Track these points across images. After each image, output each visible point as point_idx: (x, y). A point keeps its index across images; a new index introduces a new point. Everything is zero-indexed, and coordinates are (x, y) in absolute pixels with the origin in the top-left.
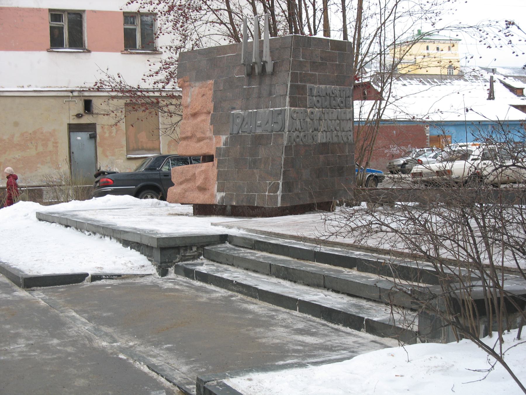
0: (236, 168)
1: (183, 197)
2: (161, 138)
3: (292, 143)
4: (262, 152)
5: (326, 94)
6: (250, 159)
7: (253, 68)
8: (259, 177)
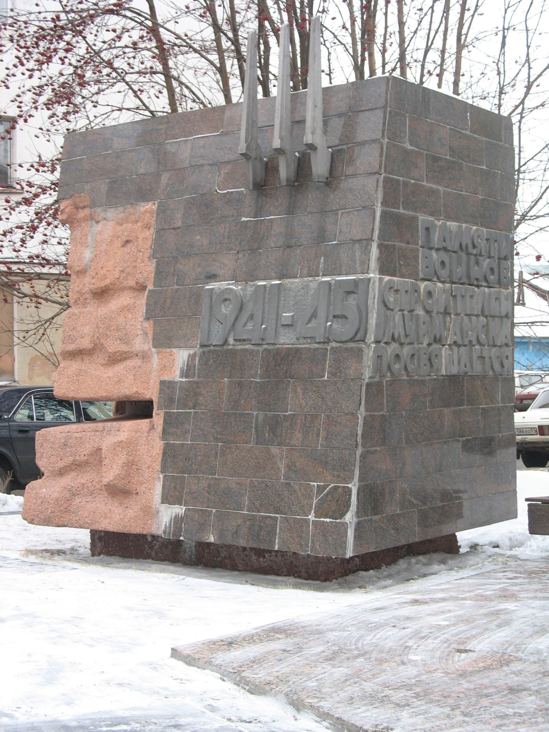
0: (216, 439)
1: (67, 511)
2: (16, 348)
3: (383, 376)
4: (295, 401)
5: (461, 245)
6: (261, 418)
7: (270, 168)
8: (288, 467)
